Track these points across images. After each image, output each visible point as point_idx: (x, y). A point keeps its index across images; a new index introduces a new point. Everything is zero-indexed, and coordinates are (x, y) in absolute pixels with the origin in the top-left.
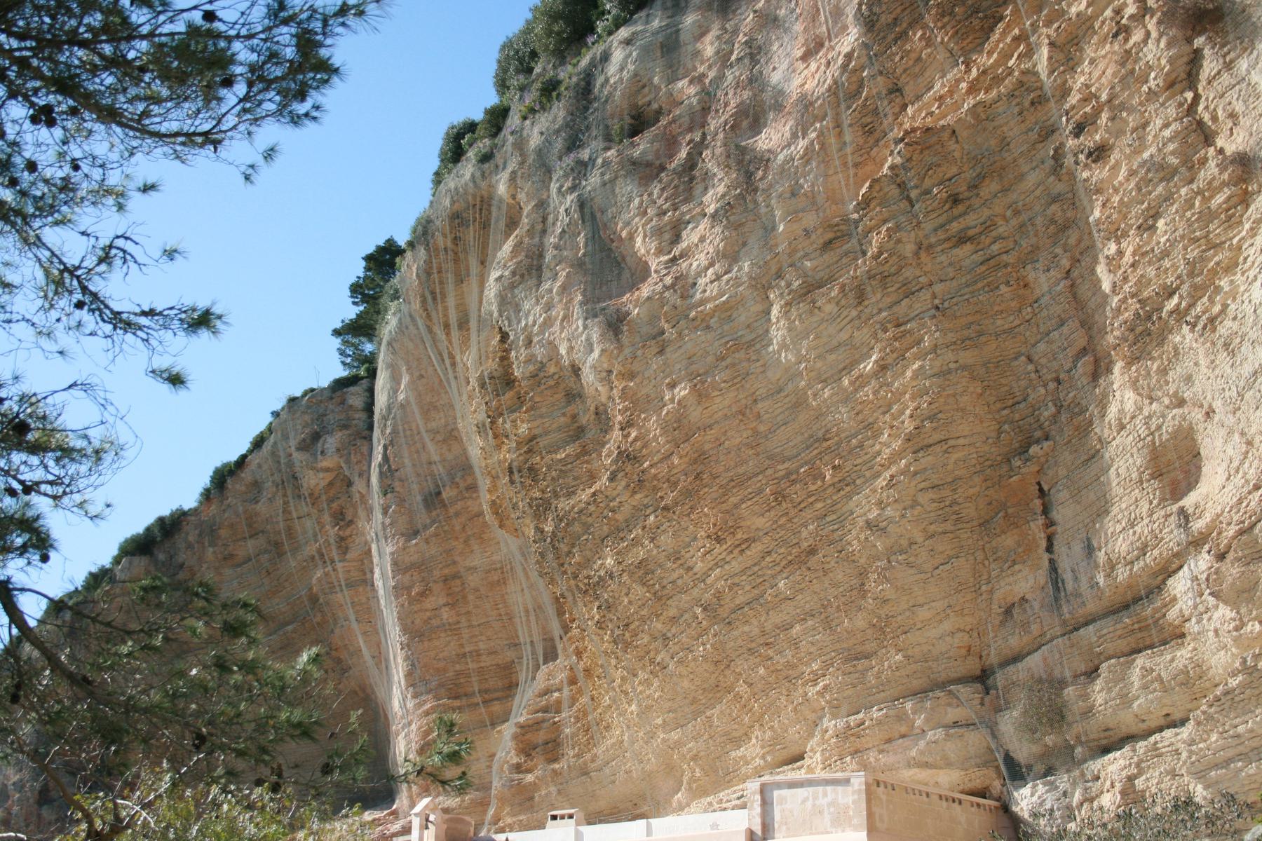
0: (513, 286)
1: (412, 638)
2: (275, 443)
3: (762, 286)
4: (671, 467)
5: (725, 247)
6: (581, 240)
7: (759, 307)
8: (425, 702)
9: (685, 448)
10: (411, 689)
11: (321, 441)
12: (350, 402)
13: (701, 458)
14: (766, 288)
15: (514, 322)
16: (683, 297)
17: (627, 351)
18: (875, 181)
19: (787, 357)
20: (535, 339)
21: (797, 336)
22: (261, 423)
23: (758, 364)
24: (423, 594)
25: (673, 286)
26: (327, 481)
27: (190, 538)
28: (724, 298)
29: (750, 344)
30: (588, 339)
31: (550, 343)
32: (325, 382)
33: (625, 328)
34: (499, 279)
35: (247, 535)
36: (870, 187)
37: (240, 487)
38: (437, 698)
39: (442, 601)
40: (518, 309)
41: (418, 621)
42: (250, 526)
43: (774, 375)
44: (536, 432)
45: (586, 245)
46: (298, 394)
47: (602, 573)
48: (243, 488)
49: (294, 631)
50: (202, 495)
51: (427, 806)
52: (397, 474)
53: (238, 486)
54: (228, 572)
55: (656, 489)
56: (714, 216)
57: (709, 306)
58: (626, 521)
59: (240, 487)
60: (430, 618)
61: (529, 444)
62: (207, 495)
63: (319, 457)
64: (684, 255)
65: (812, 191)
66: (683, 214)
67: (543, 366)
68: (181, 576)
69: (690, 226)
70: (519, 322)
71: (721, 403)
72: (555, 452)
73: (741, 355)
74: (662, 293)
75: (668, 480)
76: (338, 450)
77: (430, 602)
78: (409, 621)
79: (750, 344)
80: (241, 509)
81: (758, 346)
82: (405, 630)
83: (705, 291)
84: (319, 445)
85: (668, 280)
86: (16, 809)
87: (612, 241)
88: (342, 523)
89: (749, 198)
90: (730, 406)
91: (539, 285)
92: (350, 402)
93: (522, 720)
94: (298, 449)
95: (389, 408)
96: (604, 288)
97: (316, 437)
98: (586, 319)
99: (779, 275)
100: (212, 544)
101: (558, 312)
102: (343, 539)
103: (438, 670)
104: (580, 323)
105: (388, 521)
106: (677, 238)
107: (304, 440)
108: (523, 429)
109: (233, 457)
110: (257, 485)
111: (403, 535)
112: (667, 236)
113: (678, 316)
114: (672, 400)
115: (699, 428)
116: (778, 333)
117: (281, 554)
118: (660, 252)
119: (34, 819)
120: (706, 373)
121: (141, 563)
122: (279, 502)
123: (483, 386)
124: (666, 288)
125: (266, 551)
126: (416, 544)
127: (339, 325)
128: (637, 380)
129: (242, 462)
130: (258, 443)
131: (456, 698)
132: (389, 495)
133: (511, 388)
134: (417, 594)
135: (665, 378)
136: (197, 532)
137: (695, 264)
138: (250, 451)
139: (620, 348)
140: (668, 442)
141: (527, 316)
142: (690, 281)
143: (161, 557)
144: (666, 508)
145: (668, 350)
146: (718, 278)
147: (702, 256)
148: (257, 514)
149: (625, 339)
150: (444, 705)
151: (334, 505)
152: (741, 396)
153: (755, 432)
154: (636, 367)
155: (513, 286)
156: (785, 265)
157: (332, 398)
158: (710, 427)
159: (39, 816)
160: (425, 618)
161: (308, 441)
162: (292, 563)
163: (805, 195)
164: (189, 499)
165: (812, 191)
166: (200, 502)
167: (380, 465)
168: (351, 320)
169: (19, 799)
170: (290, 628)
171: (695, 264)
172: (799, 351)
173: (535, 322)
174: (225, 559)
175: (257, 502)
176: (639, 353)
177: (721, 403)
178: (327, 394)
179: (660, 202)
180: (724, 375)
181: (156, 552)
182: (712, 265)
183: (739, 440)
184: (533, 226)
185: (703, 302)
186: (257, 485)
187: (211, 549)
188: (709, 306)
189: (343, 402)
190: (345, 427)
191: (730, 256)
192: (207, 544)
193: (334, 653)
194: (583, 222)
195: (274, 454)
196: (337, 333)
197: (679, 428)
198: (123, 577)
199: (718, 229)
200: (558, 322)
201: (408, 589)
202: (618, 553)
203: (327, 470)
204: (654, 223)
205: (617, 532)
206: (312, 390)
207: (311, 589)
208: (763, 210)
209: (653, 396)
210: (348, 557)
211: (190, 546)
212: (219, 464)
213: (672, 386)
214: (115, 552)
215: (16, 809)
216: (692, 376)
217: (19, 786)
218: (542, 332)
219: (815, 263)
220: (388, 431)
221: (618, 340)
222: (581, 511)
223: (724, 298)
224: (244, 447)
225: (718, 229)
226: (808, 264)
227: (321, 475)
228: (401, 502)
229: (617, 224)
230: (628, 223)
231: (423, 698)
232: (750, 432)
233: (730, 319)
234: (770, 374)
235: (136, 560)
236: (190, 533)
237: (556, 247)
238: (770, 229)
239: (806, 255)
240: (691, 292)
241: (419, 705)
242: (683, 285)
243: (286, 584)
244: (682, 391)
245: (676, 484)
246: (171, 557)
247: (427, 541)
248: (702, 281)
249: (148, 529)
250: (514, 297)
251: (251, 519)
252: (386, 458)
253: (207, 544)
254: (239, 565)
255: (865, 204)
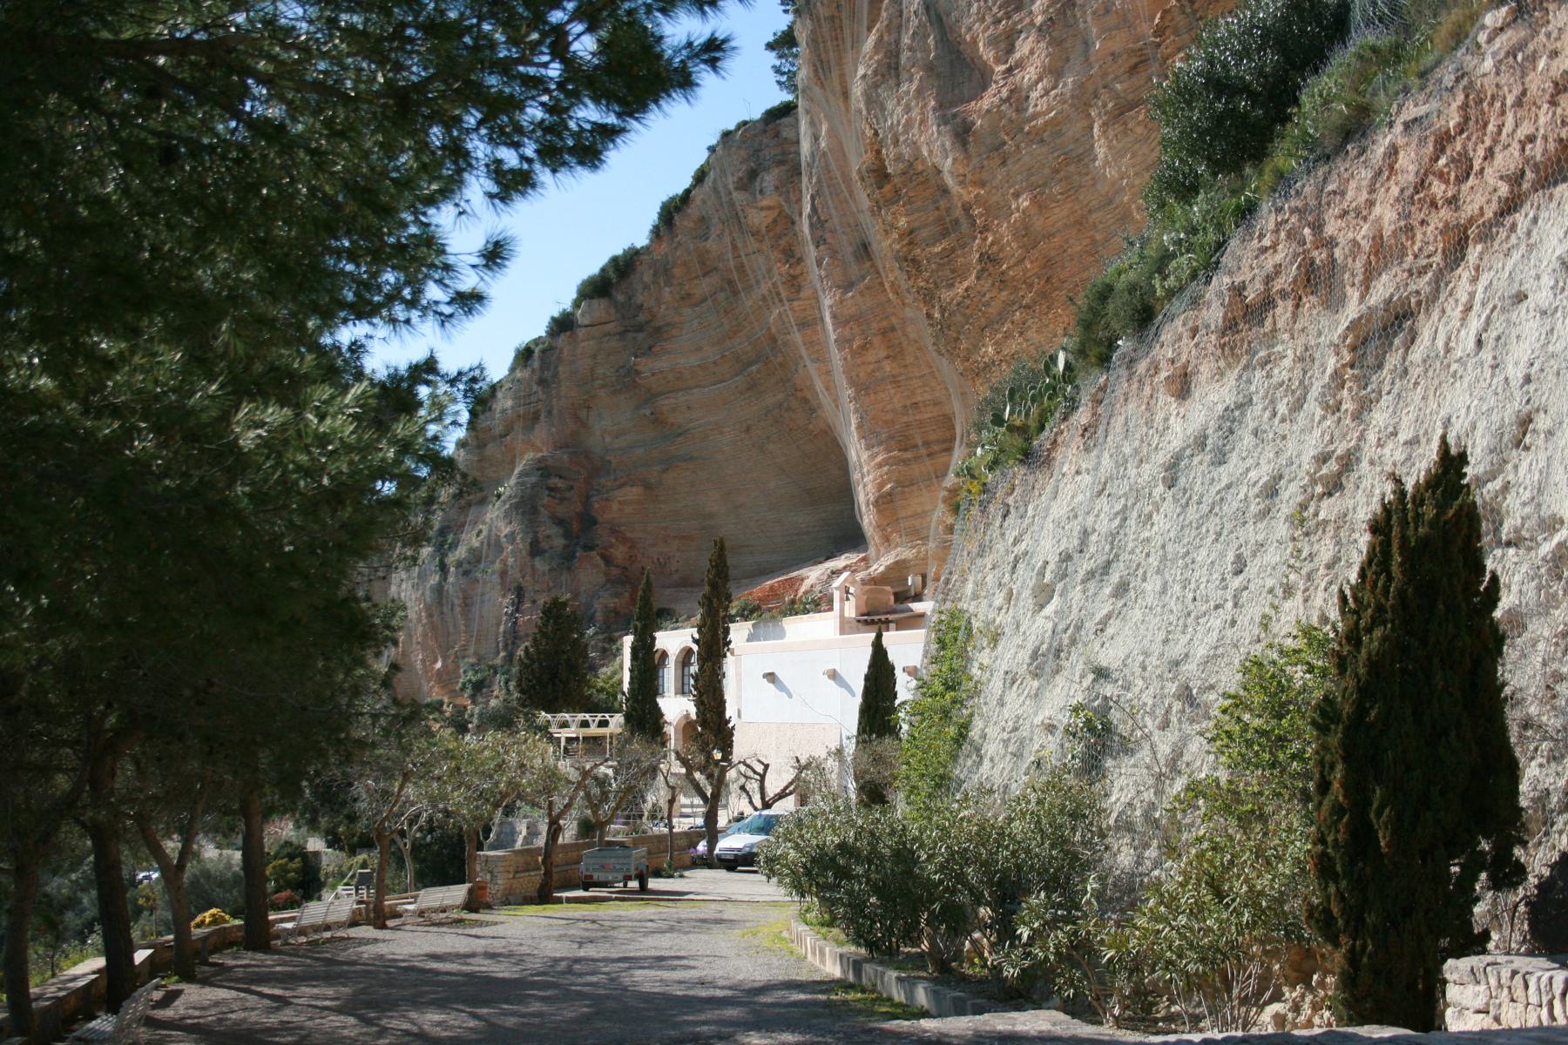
0: (876, 86)
1: (857, 392)
2: (715, 179)
3: (1083, 100)
4: (1026, 270)
5: (1050, 62)
6: (931, 41)
7: (1085, 123)
8: (877, 454)
9: (1035, 253)
10: (863, 441)
11: (759, 180)
12: (784, 134)
13: (1048, 263)
14: (1088, 105)
15: (882, 121)
16: (1018, 111)
17: (975, 161)
18: (1165, 12)
19: (1110, 173)
20: (902, 139)
21: (1118, 155)
22: (701, 157)
23: (1088, 178)
24: (864, 347)
25: (1008, 99)
26: (770, 220)
27: (646, 279)
28: (1052, 114)
29: (1080, 159)
30: (943, 145)
31: (915, 143)
32: (756, 114)
33: (971, 139)
34: (864, 76)
35: (699, 273)
36: (1162, 18)
37: (688, 224)
38: (888, 450)
39: (882, 354)
40: (883, 109)
41: (862, 374)
42: (702, 263)
43: (1103, 188)
44: (916, 224)
45: (936, 48)
46: (732, 127)
47: (986, 359)
48: (691, 225)
49: (758, 372)
50: (652, 232)
51: (846, 580)
52: (826, 225)
53: (686, 223)
54: (687, 312)
55: (1016, 289)
56: (1040, 30)
57: (1040, 121)
58: (1000, 314)
59: (688, 224)
60: (873, 371)
61: (910, 234)
62: (656, 232)
63: (758, 196)
64: (1020, 65)
65: (1123, 8)
66: (1016, 23)
67: (911, 165)
68: (642, 318)
69: (1023, 36)
70: (886, 121)
71: (1059, 214)
72: (934, 245)
73: (1072, 168)
74: (999, 107)
75: (1025, 282)
76: (777, 188)
77: (871, 356)
78: (853, 374)
79: (1080, 159)
80: (692, 247)
81: (1086, 160)
82: (852, 382)
83: (1036, 105)
84: (757, 184)
85: (1005, 93)
86: (511, 560)
87: (959, 43)
88: (792, 261)
89: (1069, 13)
90: (1068, 216)
91: (898, 85)
92: (784, 134)
93: (325, 861)
94: (736, 189)
95: (813, 155)
96: (956, 91)
97: (753, 175)
98: (939, 126)
99: (1096, 96)
100: (668, 283)
101: (915, 113)
102: (794, 277)
103: (886, 422)
104: (935, 128)
105: (823, 273)
106: (1010, 50)
107: (741, 179)
108: (902, 222)
109: (680, 191)
110: (703, 220)
111: (838, 287)
112: (1003, 46)
113: (1016, 129)
114: (1018, 209)
115: (1044, 236)
116: (1101, 151)
117: (735, 293)
118: (998, 61)
119: (529, 570)
120: (1045, 184)
121: (600, 307)
122: (728, 239)
123: (863, 179)
124: (1003, 101)
125: (722, 289)
126: (852, 297)
127: (771, 39)
128: (987, 189)
129: (688, 192)
130: (700, 177)
131: (906, 450)
132: (821, 247)
133: (889, 182)
134: (858, 347)
135: (1010, 187)
136: (651, 271)
137: (1027, 77)
138: (693, 186)
139: (968, 157)
140: (1020, 247)
141: (892, 115)
142: (1024, 94)
143: (620, 298)
144: (1027, 307)
145: (1009, 162)
146: (1047, 93)
147: (1032, 69)
148: (708, 252)
149: (972, 149)
150: (894, 457)
151: (783, 242)
152: (1077, 207)
153: (1094, 241)
154: (985, 176)
155: (876, 86)
156: (1100, 86)
157: (765, 131)
158: (1053, 235)
159: (533, 567)
160: (869, 370)
161: (745, 180)
162: (748, 303)
163: (1116, 12)
164: (641, 239)
165: (1123, 8)
166: (651, 240)
167: (810, 217)
168: (783, 32)
169: (512, 551)
170: (754, 368)
171: (1027, 77)
172: (1120, 168)
173: (899, 122)
174: (682, 299)
175: (707, 239)
176: (986, 163)
177: (1059, 214)
178: (760, 127)
179: (995, 10)
180: (1056, 189)
181: (614, 293)
182: (1040, 79)
183: (1079, 248)
184: (891, 21)
185: (1035, 116)
186: (703, 220)
187: (667, 289)
188: (1040, 121)
189: (777, 135)
190: (781, 163)
191: (1054, 72)
192: (662, 284)
193: (799, 394)
194: (930, 21)
195: (715, 190)
196: (770, 46)
197: (1024, 232)
198: (586, 322)
199: (1043, 45)
200: (917, 125)
201: (849, 341)
202: (995, 343)
203: (769, 208)
204: (990, 32)
205: (990, 325)
206: (745, 123)
207: (769, 329)
208: (1082, 26)
209: (1002, 203)
210: (802, 295)
211: (646, 287)
212: (665, 199)
213: (1017, 195)
214: (574, 296)
215: (511, 560)
216: (1032, 187)
217: (511, 537)
218: (906, 132)
219: (1126, 85)
220: (814, 180)
221: (966, 151)
222: (959, 304)
223: (1052, 114)
224: (687, 182)
225: (1043, 45)
226: (1118, 86)
227: (763, 214)
228: (834, 254)
229: (960, 28)
230: (970, 29)
231: (875, 450)
232: (1088, 241)
233: (1059, 134)
234: (1099, 187)
235: (595, 302)
236: (645, 274)
237: (910, 49)
238: (1087, 44)
239: (1116, 78)
240: (1025, 105)
241: (873, 457)
242: (1018, 98)
243: (745, 323)
244: (1024, 202)
245: (1031, 286)
246: (630, 298)
247: (862, 294)
248: (1034, 95)
249: (603, 270)
250: (878, 96)
251: (702, 257)
252: (814, 209)
253: (662, 284)
254: (696, 305)
255: (1159, 32)
